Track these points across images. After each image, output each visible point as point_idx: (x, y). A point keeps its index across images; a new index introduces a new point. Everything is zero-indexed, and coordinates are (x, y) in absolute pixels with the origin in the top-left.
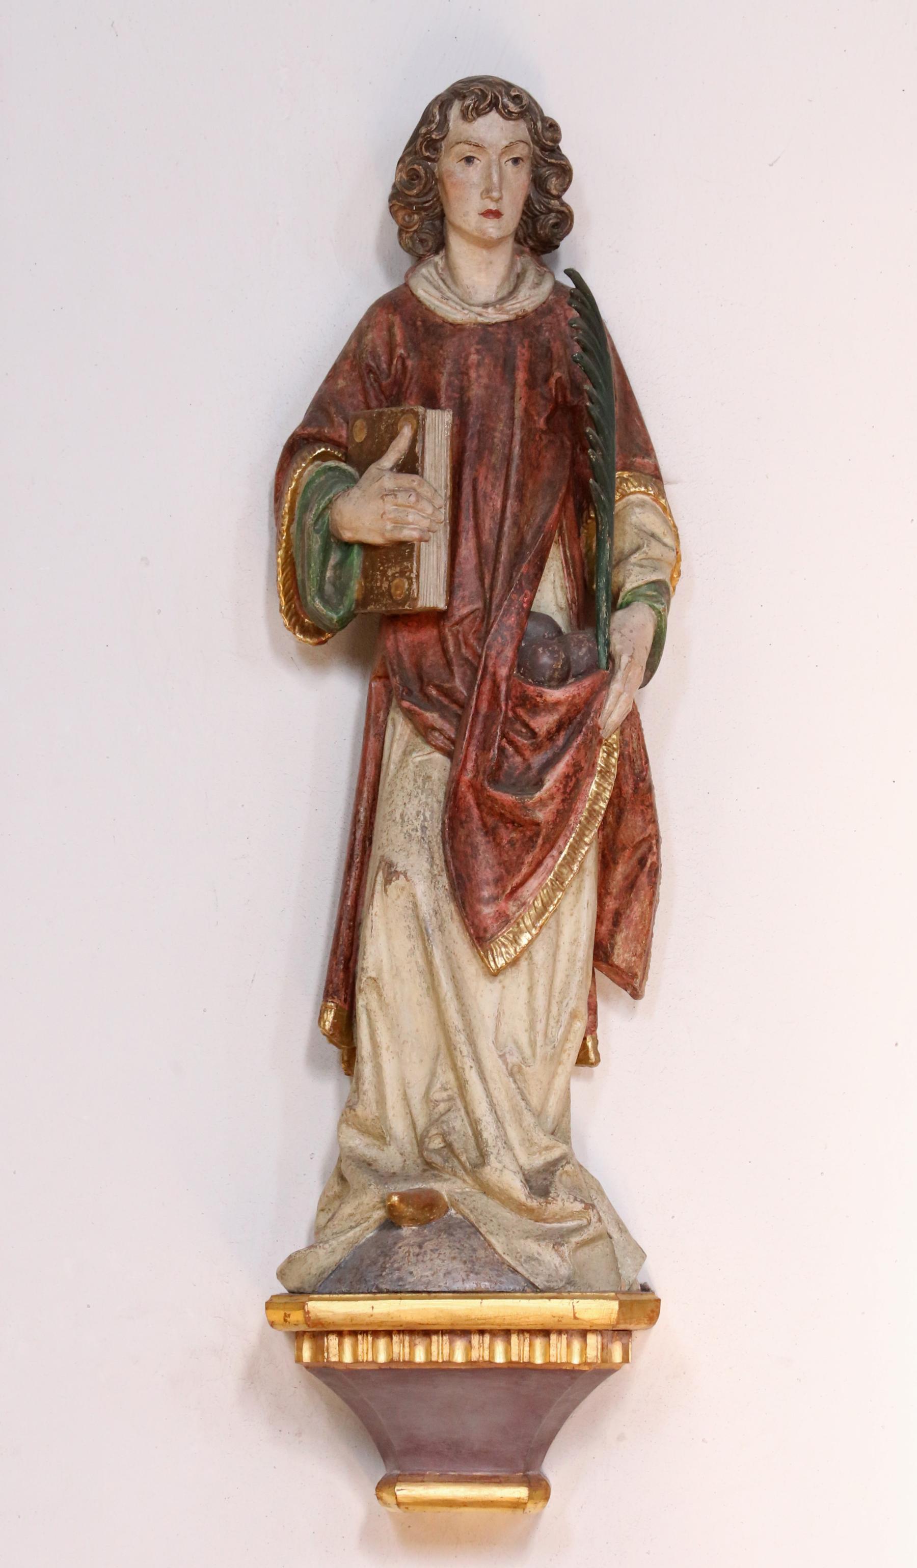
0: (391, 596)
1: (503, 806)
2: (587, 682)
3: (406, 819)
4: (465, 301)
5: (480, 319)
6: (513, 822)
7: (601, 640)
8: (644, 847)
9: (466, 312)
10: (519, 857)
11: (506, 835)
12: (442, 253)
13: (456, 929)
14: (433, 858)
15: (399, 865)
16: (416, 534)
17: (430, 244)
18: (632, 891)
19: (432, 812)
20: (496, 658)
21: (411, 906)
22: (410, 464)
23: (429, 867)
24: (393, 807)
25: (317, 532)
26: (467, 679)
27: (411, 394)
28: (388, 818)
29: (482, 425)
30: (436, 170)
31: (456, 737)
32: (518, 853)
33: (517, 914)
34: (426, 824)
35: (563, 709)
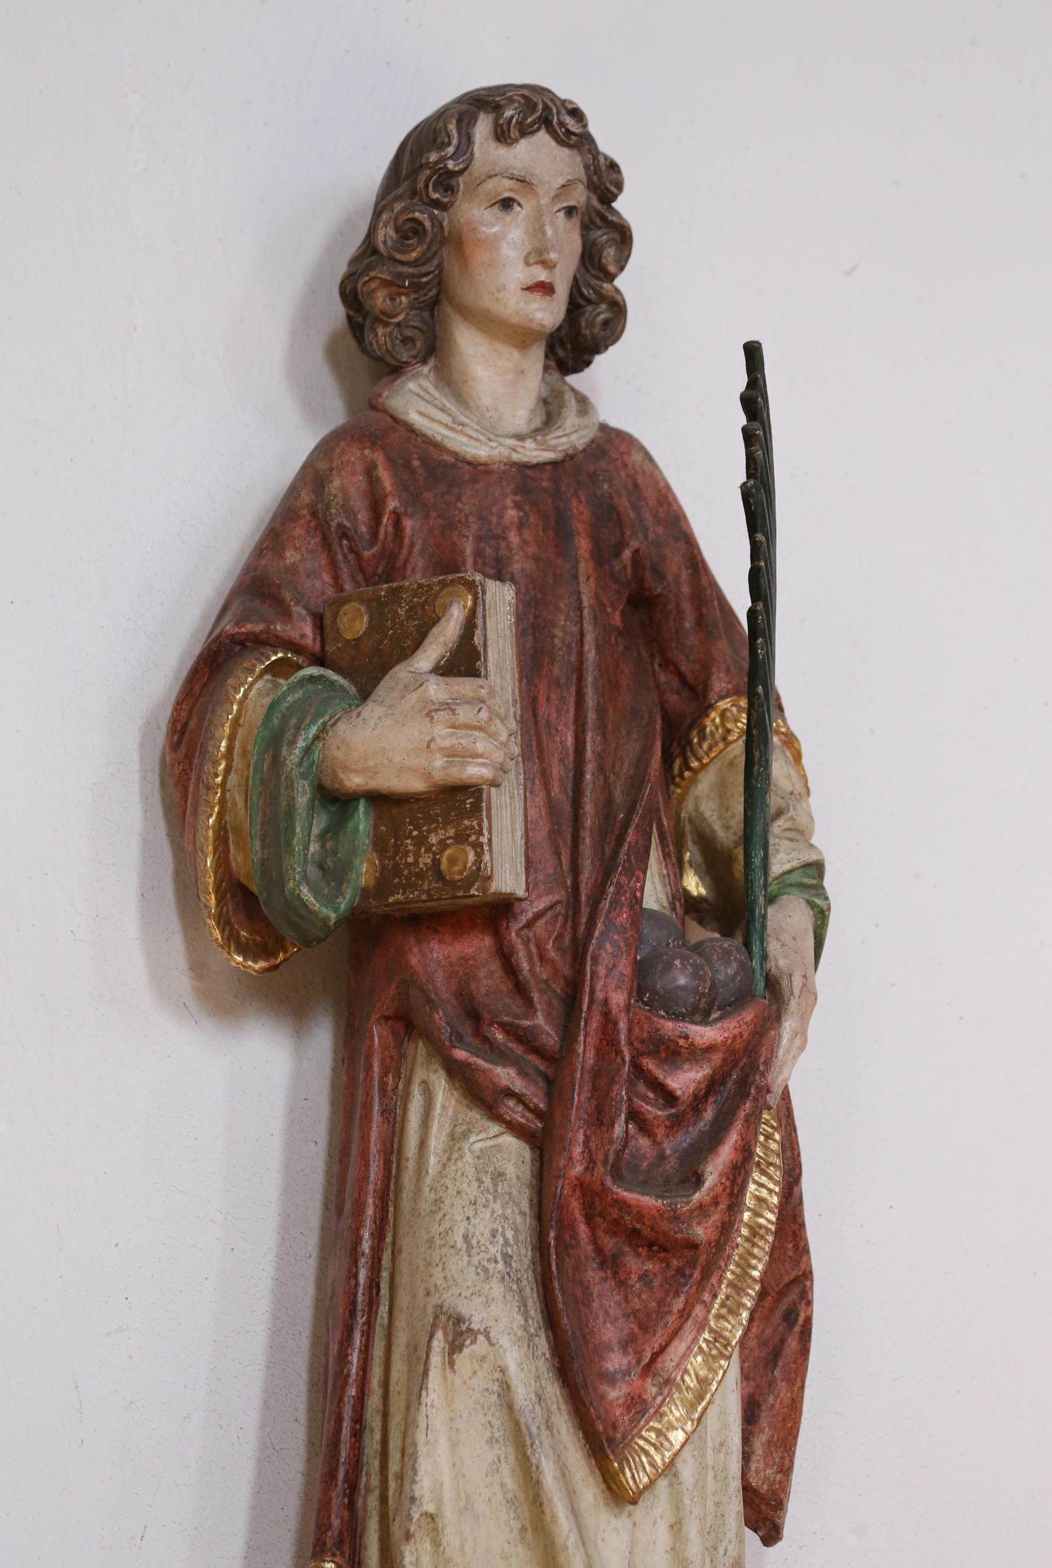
0: (439, 875)
1: (640, 1216)
2: (748, 1015)
3: (474, 1242)
4: (491, 432)
5: (515, 457)
6: (650, 1245)
7: (756, 948)
8: (793, 1295)
9: (494, 445)
10: (661, 1303)
11: (636, 1265)
12: (432, 362)
13: (564, 1426)
14: (525, 1306)
15: (475, 1319)
16: (486, 773)
17: (419, 344)
18: (775, 1366)
19: (516, 1230)
20: (606, 976)
21: (496, 1388)
22: (464, 661)
23: (523, 1322)
24: (447, 1224)
25: (304, 776)
26: (554, 1013)
27: (413, 569)
28: (438, 1242)
29: (536, 617)
30: (445, 223)
31: (550, 1104)
32: (659, 1295)
33: (659, 1399)
34: (509, 1250)
35: (717, 1058)
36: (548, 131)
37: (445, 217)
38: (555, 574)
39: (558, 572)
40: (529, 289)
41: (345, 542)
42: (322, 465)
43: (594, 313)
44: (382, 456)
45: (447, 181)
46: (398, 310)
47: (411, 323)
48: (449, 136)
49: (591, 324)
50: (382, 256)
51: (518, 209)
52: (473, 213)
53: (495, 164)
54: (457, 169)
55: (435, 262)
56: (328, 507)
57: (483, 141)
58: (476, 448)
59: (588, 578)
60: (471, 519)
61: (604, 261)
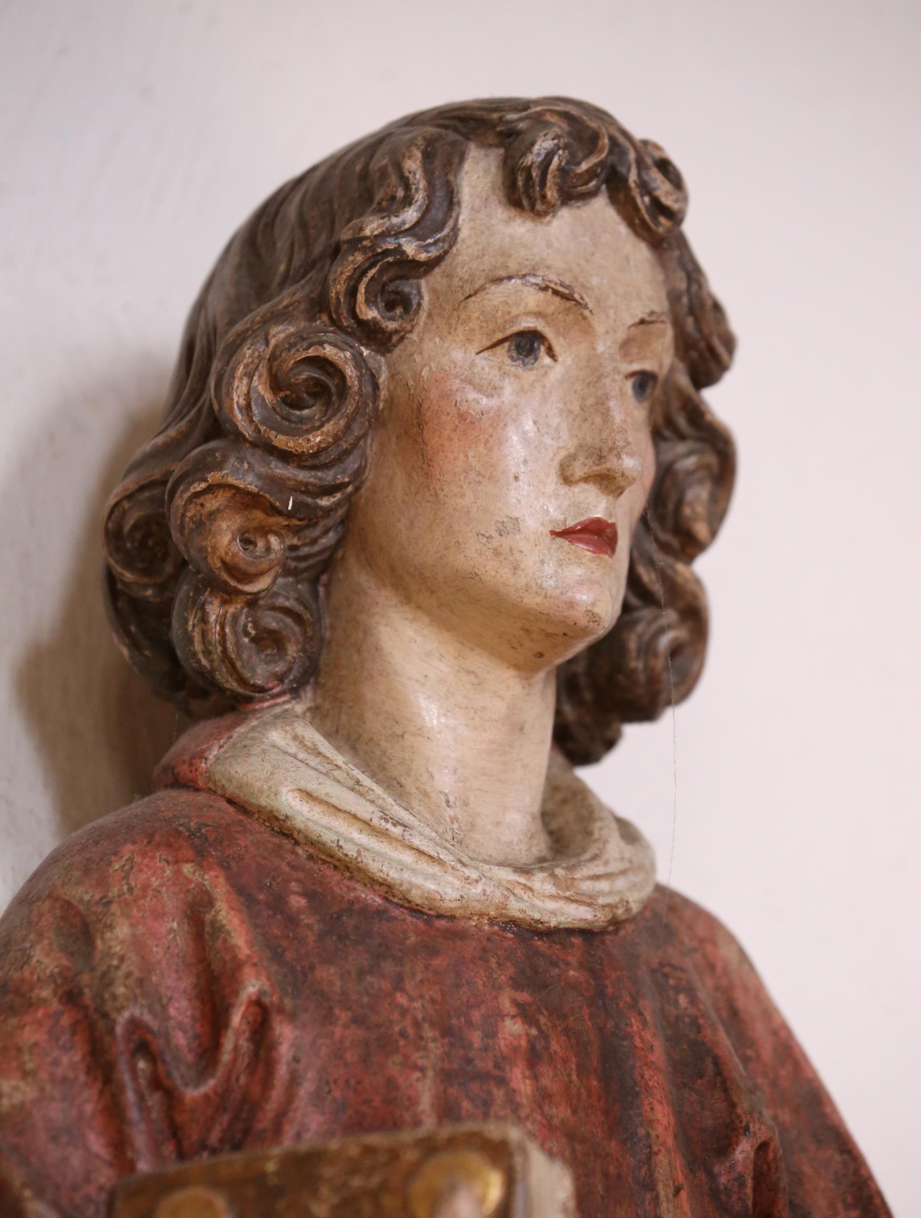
5: (515, 908)
12: (308, 694)
17: (292, 650)
30: (383, 379)
36: (613, 200)
37: (381, 364)
38: (606, 1175)
39: (612, 1170)
40: (566, 534)
41: (142, 1064)
42: (82, 894)
43: (654, 627)
44: (222, 880)
45: (397, 280)
46: (265, 566)
47: (281, 601)
48: (406, 184)
49: (648, 649)
50: (239, 437)
51: (547, 360)
52: (448, 357)
53: (505, 254)
54: (423, 257)
55: (352, 463)
56: (106, 980)
57: (477, 203)
58: (434, 877)
59: (677, 1191)
60: (429, 1033)
61: (687, 511)
